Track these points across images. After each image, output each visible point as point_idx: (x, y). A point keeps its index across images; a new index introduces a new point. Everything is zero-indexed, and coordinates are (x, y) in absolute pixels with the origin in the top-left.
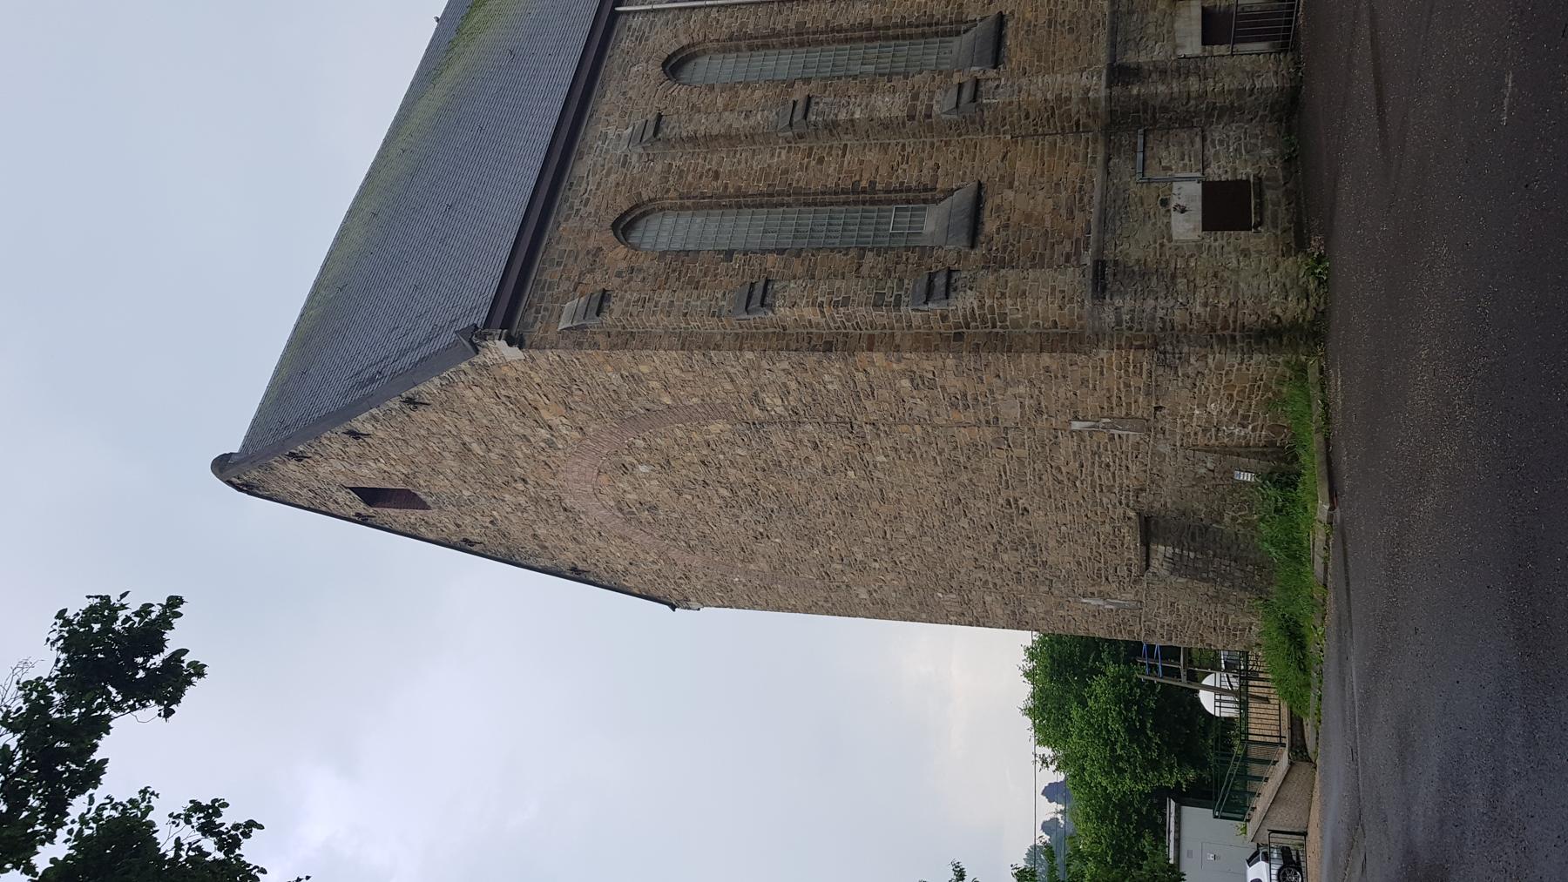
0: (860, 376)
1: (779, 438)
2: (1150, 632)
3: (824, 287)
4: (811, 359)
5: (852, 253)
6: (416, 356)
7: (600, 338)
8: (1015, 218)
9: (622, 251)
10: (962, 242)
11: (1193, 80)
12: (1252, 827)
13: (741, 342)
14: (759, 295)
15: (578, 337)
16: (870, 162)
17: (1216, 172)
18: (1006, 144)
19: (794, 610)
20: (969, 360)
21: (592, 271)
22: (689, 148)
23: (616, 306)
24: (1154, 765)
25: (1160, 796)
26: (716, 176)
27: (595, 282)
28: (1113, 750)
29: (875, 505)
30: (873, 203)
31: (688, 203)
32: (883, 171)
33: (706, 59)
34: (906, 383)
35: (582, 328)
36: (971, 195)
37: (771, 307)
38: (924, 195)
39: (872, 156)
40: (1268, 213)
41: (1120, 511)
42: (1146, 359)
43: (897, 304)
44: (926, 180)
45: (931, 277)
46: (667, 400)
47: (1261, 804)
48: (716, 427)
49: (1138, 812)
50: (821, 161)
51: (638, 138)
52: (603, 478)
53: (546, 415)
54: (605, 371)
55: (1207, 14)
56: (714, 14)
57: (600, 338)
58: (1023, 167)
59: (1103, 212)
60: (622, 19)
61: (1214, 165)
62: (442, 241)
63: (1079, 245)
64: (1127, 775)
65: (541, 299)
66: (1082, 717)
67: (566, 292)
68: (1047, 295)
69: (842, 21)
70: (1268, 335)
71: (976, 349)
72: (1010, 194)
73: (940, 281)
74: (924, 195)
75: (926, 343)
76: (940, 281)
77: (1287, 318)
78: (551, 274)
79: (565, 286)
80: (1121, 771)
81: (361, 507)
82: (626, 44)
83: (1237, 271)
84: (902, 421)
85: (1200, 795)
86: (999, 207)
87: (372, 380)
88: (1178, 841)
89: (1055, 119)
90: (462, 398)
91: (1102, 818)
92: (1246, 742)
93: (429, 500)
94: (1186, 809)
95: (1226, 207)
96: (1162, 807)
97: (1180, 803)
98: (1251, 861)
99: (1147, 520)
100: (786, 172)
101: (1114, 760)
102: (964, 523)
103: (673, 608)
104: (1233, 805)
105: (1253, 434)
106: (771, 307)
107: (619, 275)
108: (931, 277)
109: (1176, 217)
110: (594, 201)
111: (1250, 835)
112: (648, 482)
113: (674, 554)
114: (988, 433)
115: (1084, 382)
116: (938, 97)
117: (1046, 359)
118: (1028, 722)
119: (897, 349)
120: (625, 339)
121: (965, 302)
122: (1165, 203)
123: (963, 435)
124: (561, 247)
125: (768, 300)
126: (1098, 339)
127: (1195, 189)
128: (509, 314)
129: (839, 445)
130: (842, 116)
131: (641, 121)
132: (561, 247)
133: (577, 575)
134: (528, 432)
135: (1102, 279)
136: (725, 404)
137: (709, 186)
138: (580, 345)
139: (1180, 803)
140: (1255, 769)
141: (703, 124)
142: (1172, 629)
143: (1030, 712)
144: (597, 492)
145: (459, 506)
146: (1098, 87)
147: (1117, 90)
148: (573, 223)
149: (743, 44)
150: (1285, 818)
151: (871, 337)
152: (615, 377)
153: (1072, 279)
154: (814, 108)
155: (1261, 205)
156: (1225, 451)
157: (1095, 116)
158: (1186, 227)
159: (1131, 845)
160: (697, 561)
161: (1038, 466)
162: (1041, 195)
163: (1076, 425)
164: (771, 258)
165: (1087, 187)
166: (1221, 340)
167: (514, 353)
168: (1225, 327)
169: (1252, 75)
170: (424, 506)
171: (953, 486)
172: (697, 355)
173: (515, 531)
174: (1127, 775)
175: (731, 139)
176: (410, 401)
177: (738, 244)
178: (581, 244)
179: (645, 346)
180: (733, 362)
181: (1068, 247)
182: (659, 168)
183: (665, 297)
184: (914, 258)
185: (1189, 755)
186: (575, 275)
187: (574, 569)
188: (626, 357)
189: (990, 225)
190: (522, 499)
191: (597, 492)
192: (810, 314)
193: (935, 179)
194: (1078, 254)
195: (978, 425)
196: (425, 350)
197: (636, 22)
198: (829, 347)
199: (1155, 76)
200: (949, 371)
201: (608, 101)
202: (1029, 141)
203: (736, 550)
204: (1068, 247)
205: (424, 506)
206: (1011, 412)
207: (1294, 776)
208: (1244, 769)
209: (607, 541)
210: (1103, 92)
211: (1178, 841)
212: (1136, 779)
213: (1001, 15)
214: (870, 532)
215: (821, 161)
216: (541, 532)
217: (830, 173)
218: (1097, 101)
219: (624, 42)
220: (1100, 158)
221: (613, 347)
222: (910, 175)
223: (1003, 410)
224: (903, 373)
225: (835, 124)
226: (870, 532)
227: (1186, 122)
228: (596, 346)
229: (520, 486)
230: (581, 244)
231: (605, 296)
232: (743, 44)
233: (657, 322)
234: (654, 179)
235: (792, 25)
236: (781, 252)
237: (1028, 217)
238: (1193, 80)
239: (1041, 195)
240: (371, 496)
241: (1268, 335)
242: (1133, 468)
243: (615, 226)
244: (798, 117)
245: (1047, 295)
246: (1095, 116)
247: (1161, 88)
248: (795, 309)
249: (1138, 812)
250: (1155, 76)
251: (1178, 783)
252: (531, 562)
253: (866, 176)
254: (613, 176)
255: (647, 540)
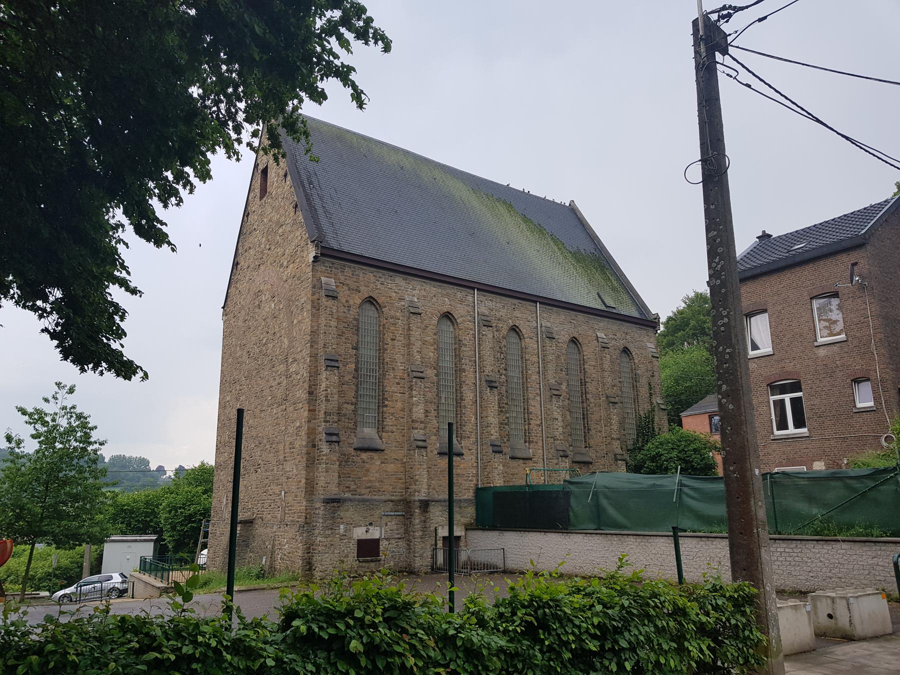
0: (301, 405)
1: (282, 368)
2: (214, 525)
3: (335, 391)
4: (306, 386)
5: (354, 400)
6: (318, 206)
7: (317, 296)
8: (367, 466)
9: (358, 301)
10: (356, 445)
11: (421, 533)
12: (137, 574)
13: (314, 356)
14: (332, 363)
15: (317, 286)
16: (396, 404)
17: (383, 545)
18: (402, 460)
19: (222, 366)
20: (304, 450)
21: (349, 289)
22: (406, 327)
23: (330, 303)
24: (173, 528)
25: (159, 532)
26: (393, 340)
27: (343, 294)
28: (180, 508)
29: (259, 407)
30: (379, 406)
31: (381, 328)
32: (392, 410)
33: (452, 330)
34: (298, 424)
35: (321, 288)
36: (378, 447)
37: (326, 370)
38: (381, 427)
39: (399, 405)
40: (364, 564)
41: (256, 511)
42: (302, 520)
43: (325, 422)
44: (387, 428)
45: (337, 435)
46: (295, 322)
47: (146, 577)
48: (286, 341)
49: (151, 521)
50: (398, 384)
51: (412, 304)
52: (270, 287)
53: (291, 266)
54: (305, 296)
55: (376, 542)
56: (471, 332)
57: (317, 296)
58: (391, 467)
59: (368, 500)
60: (471, 291)
61: (387, 543)
62: (378, 210)
63: (354, 492)
64: (167, 515)
65: (336, 268)
66: (197, 492)
67: (339, 279)
68: (328, 481)
69: (465, 388)
70: (309, 566)
71: (308, 453)
72: (378, 463)
73: (334, 438)
74: (381, 427)
75: (311, 433)
76: (334, 438)
77: (315, 573)
78: (348, 272)
79: (342, 278)
80: (170, 512)
81: (261, 167)
82: (459, 295)
83: (333, 553)
84: (286, 422)
85: (161, 551)
86: (372, 459)
87: (310, 183)
88: (136, 541)
89: (409, 480)
90: (297, 230)
91: (147, 503)
92: (168, 570)
93: (263, 201)
94: (152, 544)
95: (368, 549)
96: (154, 532)
97: (156, 541)
98: (122, 575)
99: (252, 522)
100: (394, 369)
101: (175, 509)
102: (253, 445)
103: (223, 308)
104: (145, 566)
105: (279, 564)
106: (326, 370)
107: (347, 301)
108: (337, 435)
109: (364, 529)
110: (382, 287)
111: (133, 573)
112: (269, 307)
113: (243, 312)
114: (281, 457)
115: (296, 496)
116: (421, 431)
117: (304, 481)
118: (197, 464)
119: (309, 421)
120: (316, 307)
121: (325, 448)
122: (371, 524)
123: (281, 447)
124: (361, 275)
125: (329, 368)
126: (310, 501)
127: (377, 536)
128: (328, 255)
129: (279, 394)
130: (414, 392)
131: (419, 304)
132: (361, 275)
133: (235, 264)
134: (286, 256)
135: (333, 502)
136: (293, 347)
137: (388, 337)
138: (314, 287)
139: (156, 541)
140: (159, 574)
141: (416, 333)
142: (214, 534)
143: (203, 464)
144: (265, 282)
145: (261, 215)
146: (422, 496)
147: (418, 504)
148: (373, 279)
149: (457, 346)
150: (139, 588)
151: (315, 410)
152: (302, 301)
153: (334, 490)
154: (419, 380)
155: (368, 561)
156: (273, 553)
157: (410, 495)
158: (360, 533)
159: (133, 518)
160: (240, 323)
161: (271, 478)
162: (378, 475)
163: (283, 493)
164: (353, 366)
165: (380, 493)
166: (309, 548)
167: (311, 259)
168: (314, 549)
169: (421, 556)
170: (261, 198)
171: (265, 441)
172: (309, 338)
173: (251, 239)
174: (167, 515)
175: (409, 345)
176: (296, 206)
177: (362, 351)
178: (362, 283)
179: (313, 316)
180: (306, 352)
181: (353, 487)
182: (398, 314)
183: (333, 323)
184: (351, 425)
185: (179, 545)
186: (348, 282)
187: (237, 264)
188: (309, 307)
189: (364, 456)
190: (262, 246)
191: (265, 282)
192: (324, 385)
193: (387, 432)
194: (350, 491)
195: (285, 453)
196: (320, 211)
197: (470, 298)
198: (310, 393)
199: (423, 518)
200: (301, 442)
201: (432, 289)
202: (403, 469)
203: (244, 342)
204: (353, 487)
205: (261, 198)
206: (288, 467)
207: (155, 590)
208: (166, 570)
209: (248, 282)
210: (417, 498)
211: (136, 541)
212: (166, 519)
213: (463, 455)
214: (250, 404)
215: (398, 384)
216: (252, 252)
217: (391, 387)
218: (414, 495)
219: (460, 293)
220: (393, 498)
221: (313, 302)
222: (389, 422)
223: (289, 463)
224: (301, 423)
225: (412, 390)
226: (250, 404)
227: (406, 531)
228: (313, 294)
229: (268, 247)
230: (362, 283)
231: (335, 298)
232: (457, 346)
233: (323, 321)
234: (392, 313)
235: (464, 366)
236: (356, 370)
237: (368, 470)
238: (421, 533)
239: (378, 475)
240: (265, 172)
241: (309, 566)
242: (269, 516)
243: (371, 297)
244: (415, 374)
245: (328, 481)
246: (410, 495)
247: (417, 521)
248: (326, 380)
249: (151, 521)
250: (423, 518)
251: (165, 540)
252: (240, 244)
253: (390, 403)
254: (394, 294)
255: (248, 301)
